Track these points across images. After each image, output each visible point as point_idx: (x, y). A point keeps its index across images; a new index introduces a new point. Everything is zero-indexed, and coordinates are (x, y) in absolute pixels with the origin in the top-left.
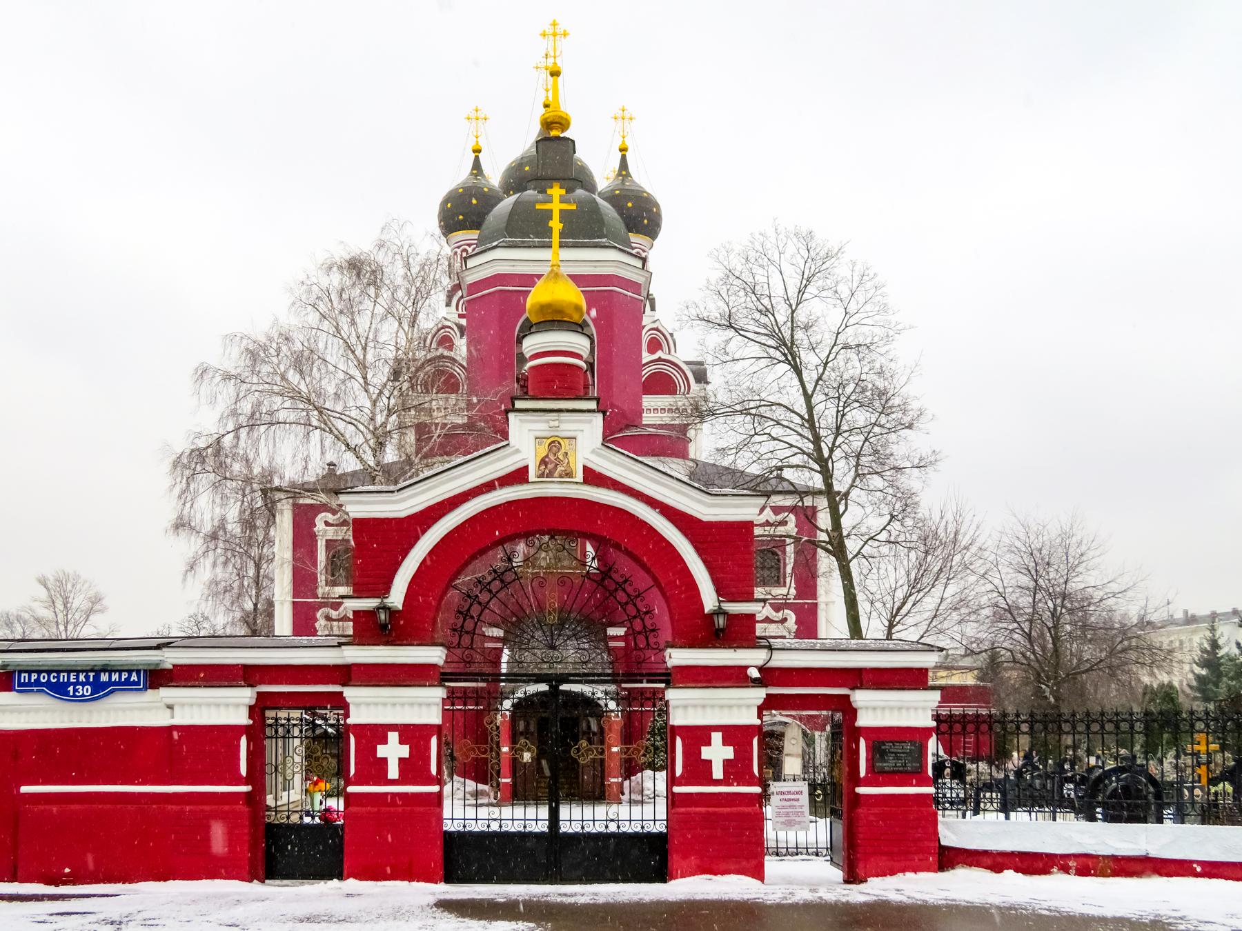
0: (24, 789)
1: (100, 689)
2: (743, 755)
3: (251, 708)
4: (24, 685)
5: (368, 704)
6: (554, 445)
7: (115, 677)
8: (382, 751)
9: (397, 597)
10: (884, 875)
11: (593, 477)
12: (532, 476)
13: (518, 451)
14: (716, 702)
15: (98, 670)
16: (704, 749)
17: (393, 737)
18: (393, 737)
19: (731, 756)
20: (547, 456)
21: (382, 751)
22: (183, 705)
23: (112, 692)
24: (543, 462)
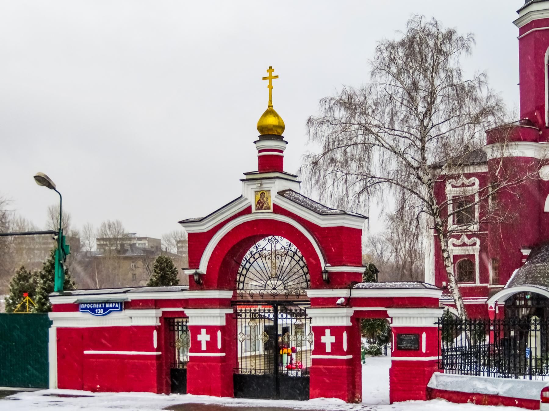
0: (86, 352)
1: (107, 311)
3: (352, 318)
6: (263, 194)
7: (111, 306)
9: (203, 268)
10: (401, 401)
11: (277, 209)
12: (253, 210)
13: (246, 199)
14: (340, 315)
15: (106, 302)
19: (334, 341)
20: (260, 200)
23: (110, 312)
24: (258, 203)
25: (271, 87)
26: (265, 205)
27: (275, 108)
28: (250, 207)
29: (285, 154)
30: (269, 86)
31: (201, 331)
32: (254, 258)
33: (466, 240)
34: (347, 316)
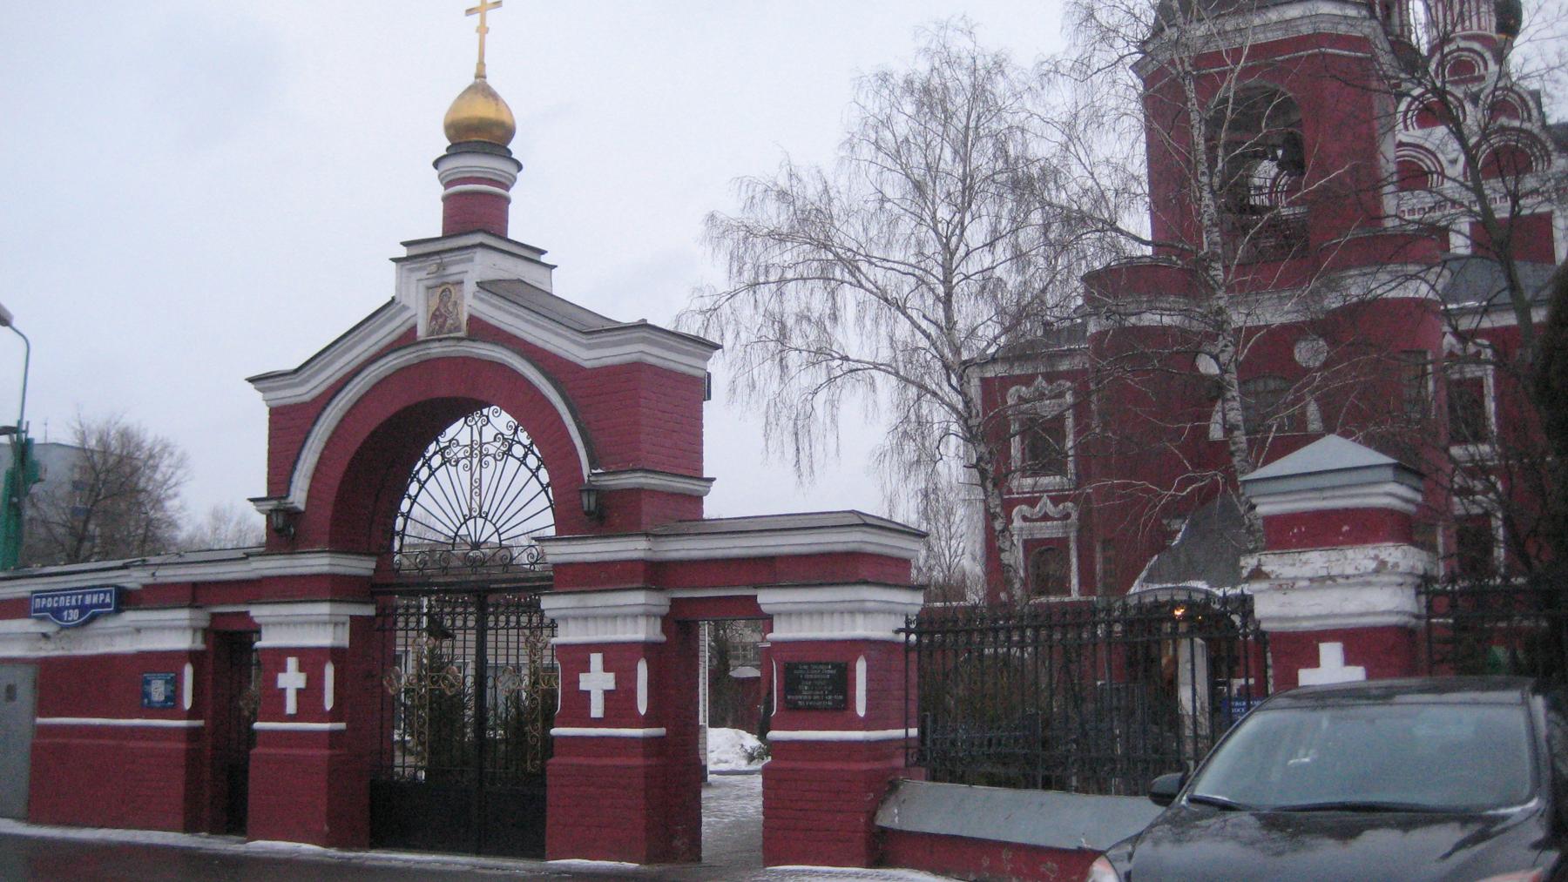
11: (479, 330)
13: (405, 308)
24: (434, 317)
25: (483, 30)
26: (450, 322)
27: (492, 81)
28: (413, 329)
29: (513, 193)
30: (487, 30)
32: (430, 467)
33: (1050, 509)
34: (648, 615)
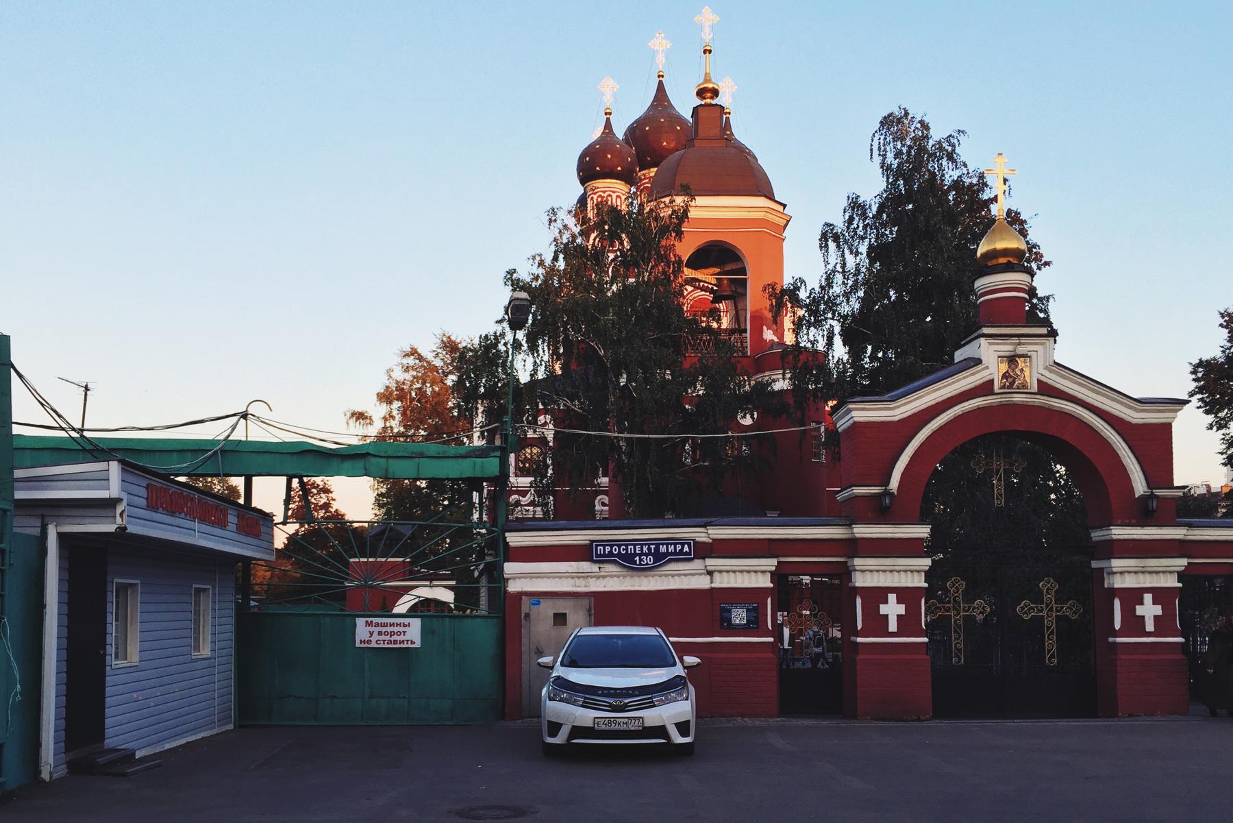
2: (912, 611)
4: (600, 556)
5: (871, 571)
7: (671, 549)
8: (883, 609)
9: (894, 484)
13: (987, 368)
15: (658, 542)
16: (1160, 613)
17: (892, 597)
18: (892, 597)
21: (883, 609)
22: (720, 572)
24: (1005, 376)
31: (1142, 598)
